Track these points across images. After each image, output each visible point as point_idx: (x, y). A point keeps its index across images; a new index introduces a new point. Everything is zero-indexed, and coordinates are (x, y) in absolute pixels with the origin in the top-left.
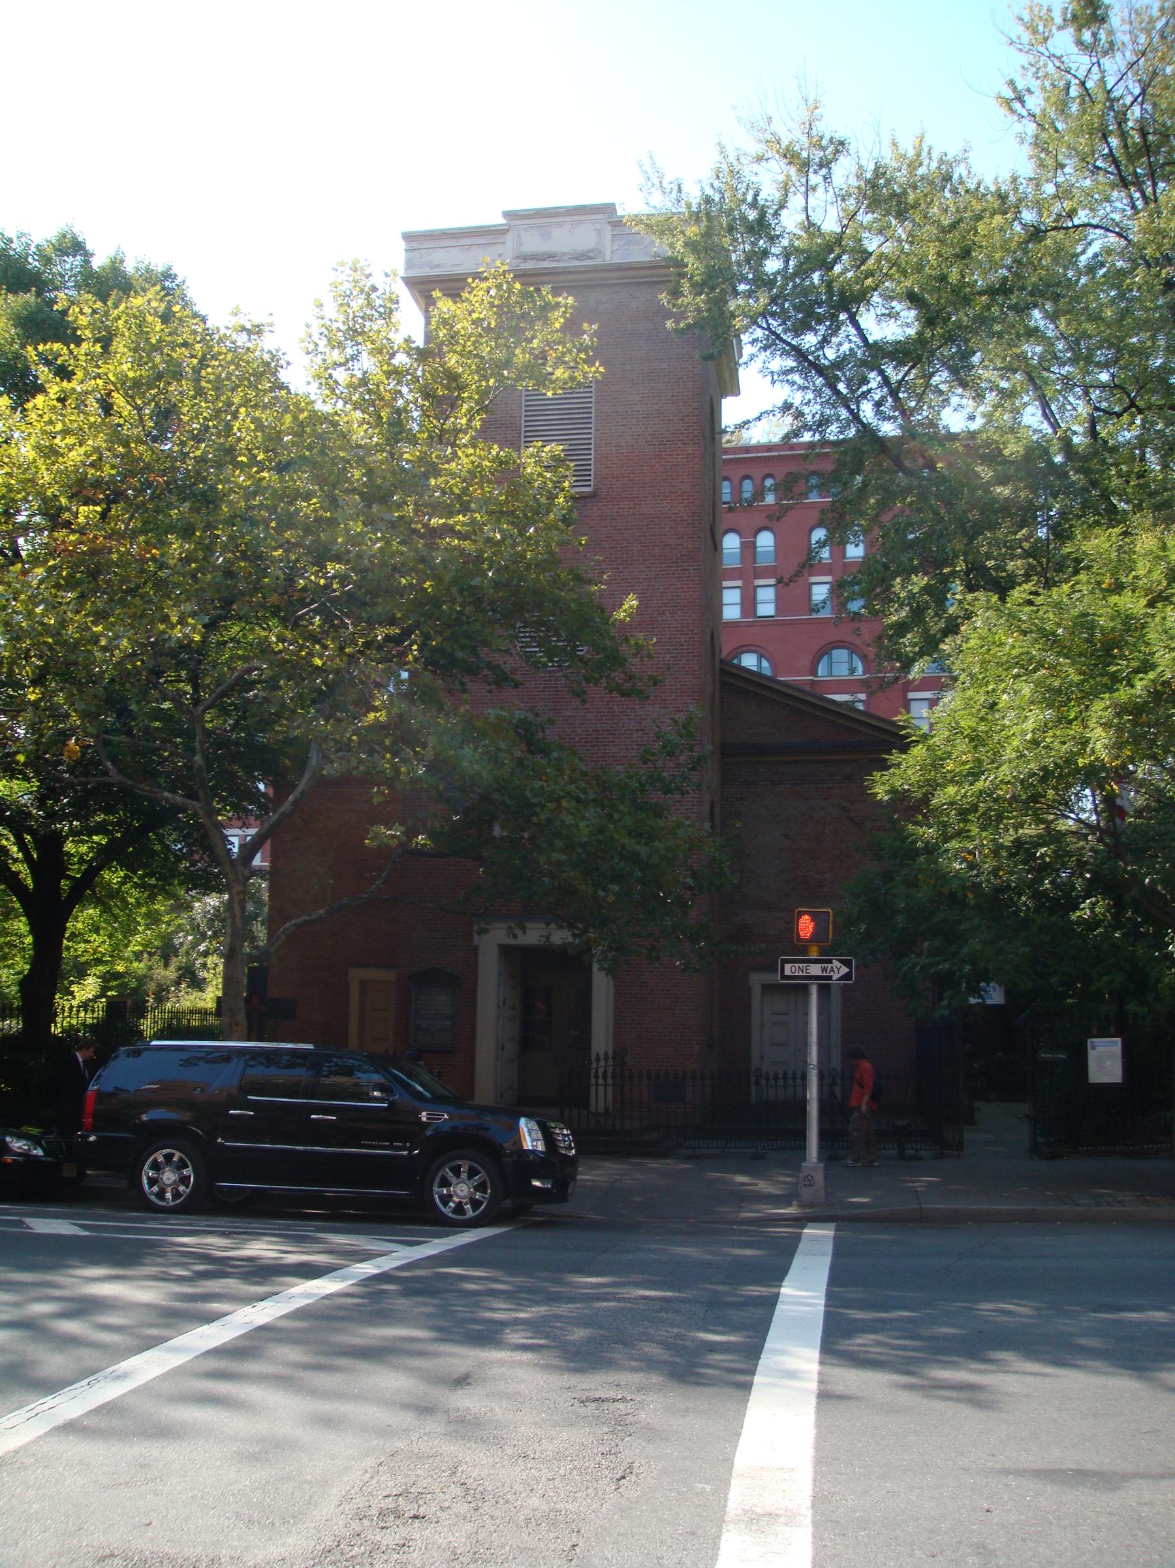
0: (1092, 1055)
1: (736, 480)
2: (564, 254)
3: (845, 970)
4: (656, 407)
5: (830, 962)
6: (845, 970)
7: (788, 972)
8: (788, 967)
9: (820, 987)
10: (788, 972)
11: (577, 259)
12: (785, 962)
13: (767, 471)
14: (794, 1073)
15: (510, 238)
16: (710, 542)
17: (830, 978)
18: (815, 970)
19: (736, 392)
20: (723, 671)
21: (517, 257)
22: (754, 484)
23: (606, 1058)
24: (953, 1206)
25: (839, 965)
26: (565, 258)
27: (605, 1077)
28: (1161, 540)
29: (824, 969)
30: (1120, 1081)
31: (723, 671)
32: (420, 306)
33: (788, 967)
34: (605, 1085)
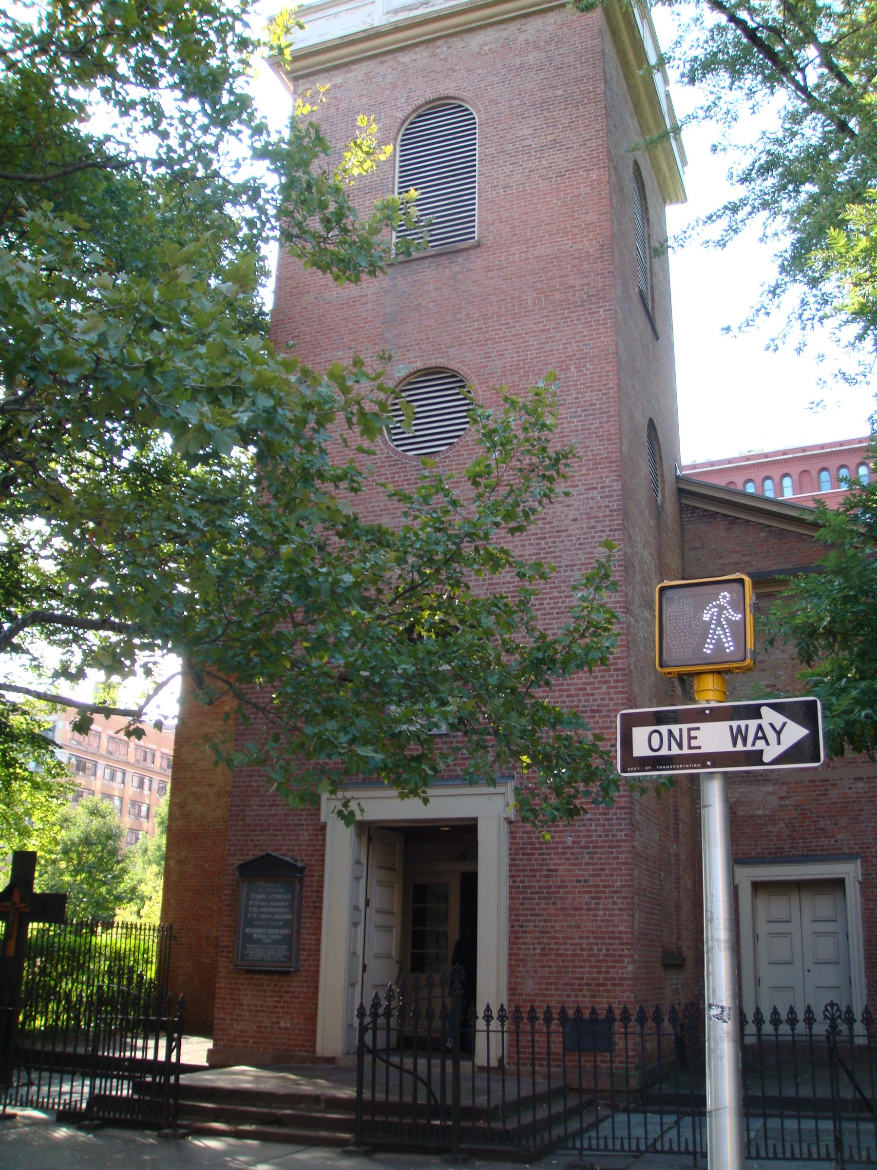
1: (758, 481)
3: (795, 732)
4: (553, 137)
5: (754, 712)
6: (795, 732)
7: (640, 749)
9: (729, 780)
10: (640, 749)
13: (785, 471)
17: (756, 757)
19: (680, 197)
20: (681, 491)
22: (774, 484)
25: (778, 719)
29: (737, 735)
31: (681, 491)
32: (288, 89)
33: (640, 734)
34: (388, 1029)
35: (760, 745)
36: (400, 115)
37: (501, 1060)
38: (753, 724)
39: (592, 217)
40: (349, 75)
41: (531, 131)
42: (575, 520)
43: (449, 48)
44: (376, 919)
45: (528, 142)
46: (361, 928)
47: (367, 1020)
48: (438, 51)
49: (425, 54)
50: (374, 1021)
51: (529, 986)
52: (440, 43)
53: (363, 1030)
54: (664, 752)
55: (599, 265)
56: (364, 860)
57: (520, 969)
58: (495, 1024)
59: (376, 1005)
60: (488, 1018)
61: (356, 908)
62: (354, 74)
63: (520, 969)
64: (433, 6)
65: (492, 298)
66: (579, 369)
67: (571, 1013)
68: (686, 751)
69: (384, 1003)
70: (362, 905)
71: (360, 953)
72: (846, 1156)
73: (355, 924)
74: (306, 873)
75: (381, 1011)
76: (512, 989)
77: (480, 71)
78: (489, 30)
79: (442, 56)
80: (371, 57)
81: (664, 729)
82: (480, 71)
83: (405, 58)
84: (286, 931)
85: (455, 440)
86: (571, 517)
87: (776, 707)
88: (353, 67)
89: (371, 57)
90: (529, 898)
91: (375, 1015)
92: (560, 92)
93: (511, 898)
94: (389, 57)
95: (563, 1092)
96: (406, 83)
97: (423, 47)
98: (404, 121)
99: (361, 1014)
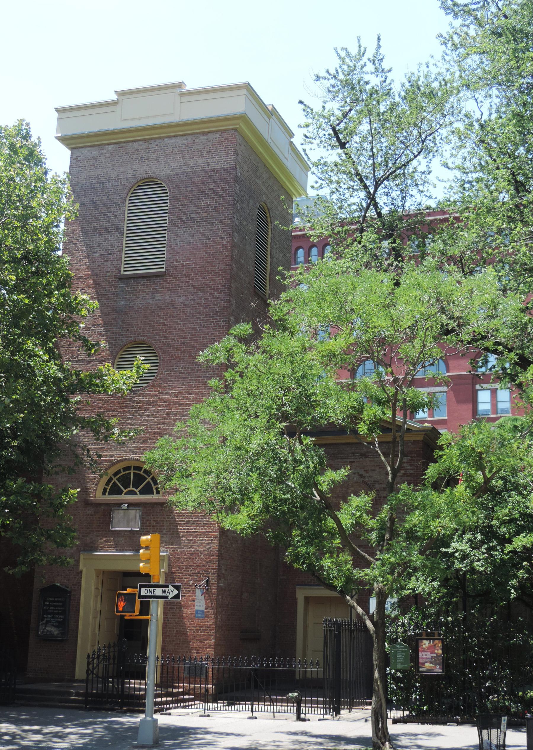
4: (205, 214)
5: (167, 586)
7: (143, 594)
8: (143, 589)
10: (143, 594)
17: (166, 597)
25: (172, 588)
29: (164, 592)
33: (143, 589)
35: (168, 594)
38: (167, 589)
41: (195, 209)
45: (193, 215)
47: (91, 660)
53: (89, 663)
54: (148, 594)
57: (167, 640)
63: (167, 640)
68: (152, 595)
72: (254, 710)
74: (73, 593)
81: (148, 589)
90: (172, 608)
91: (93, 658)
92: (211, 187)
99: (88, 657)
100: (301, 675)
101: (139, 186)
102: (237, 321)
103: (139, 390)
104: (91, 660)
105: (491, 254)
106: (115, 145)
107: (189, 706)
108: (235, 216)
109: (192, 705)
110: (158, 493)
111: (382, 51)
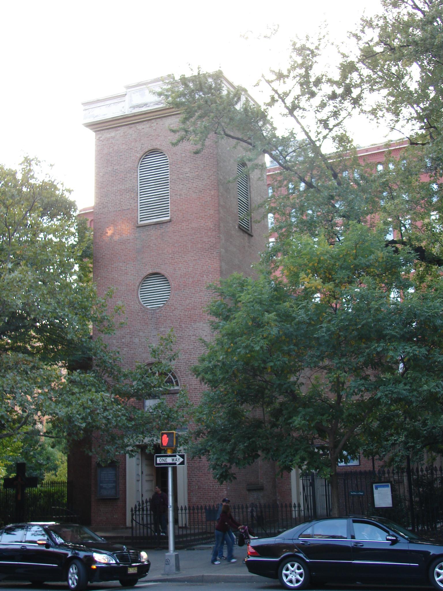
0: (376, 495)
2: (151, 103)
4: (197, 173)
5: (175, 456)
7: (158, 462)
8: (158, 459)
10: (158, 462)
11: (157, 104)
12: (157, 457)
14: (238, 506)
15: (127, 98)
16: (147, 228)
17: (175, 464)
18: (169, 460)
21: (131, 107)
23: (147, 502)
24: (217, 574)
26: (151, 105)
27: (147, 510)
28: (328, 117)
29: (173, 460)
30: (391, 506)
33: (158, 459)
34: (147, 514)
36: (139, 156)
37: (186, 524)
38: (175, 458)
39: (212, 212)
40: (117, 132)
42: (206, 336)
43: (157, 124)
44: (145, 478)
45: (188, 175)
46: (140, 481)
47: (134, 512)
48: (152, 125)
49: (148, 126)
50: (135, 513)
51: (194, 499)
52: (153, 121)
55: (214, 233)
56: (140, 458)
58: (184, 511)
59: (136, 508)
60: (182, 509)
61: (138, 475)
62: (119, 132)
64: (149, 106)
65: (176, 245)
66: (207, 276)
67: (208, 507)
69: (138, 507)
70: (140, 474)
71: (140, 490)
73: (138, 481)
75: (137, 509)
76: (189, 501)
77: (169, 138)
78: (173, 117)
79: (154, 128)
80: (126, 125)
82: (169, 138)
83: (140, 127)
84: (114, 484)
85: (165, 302)
86: (205, 335)
87: (179, 455)
88: (119, 128)
89: (126, 125)
91: (136, 511)
93: (188, 470)
94: (133, 125)
95: (206, 533)
96: (140, 140)
97: (146, 122)
98: (140, 159)
100: (27, 583)
101: (146, 156)
102: (361, 328)
103: (157, 309)
104: (134, 512)
105: (362, 81)
106: (131, 131)
107: (211, 542)
108: (219, 173)
109: (213, 541)
110: (177, 385)
111: (363, 95)
